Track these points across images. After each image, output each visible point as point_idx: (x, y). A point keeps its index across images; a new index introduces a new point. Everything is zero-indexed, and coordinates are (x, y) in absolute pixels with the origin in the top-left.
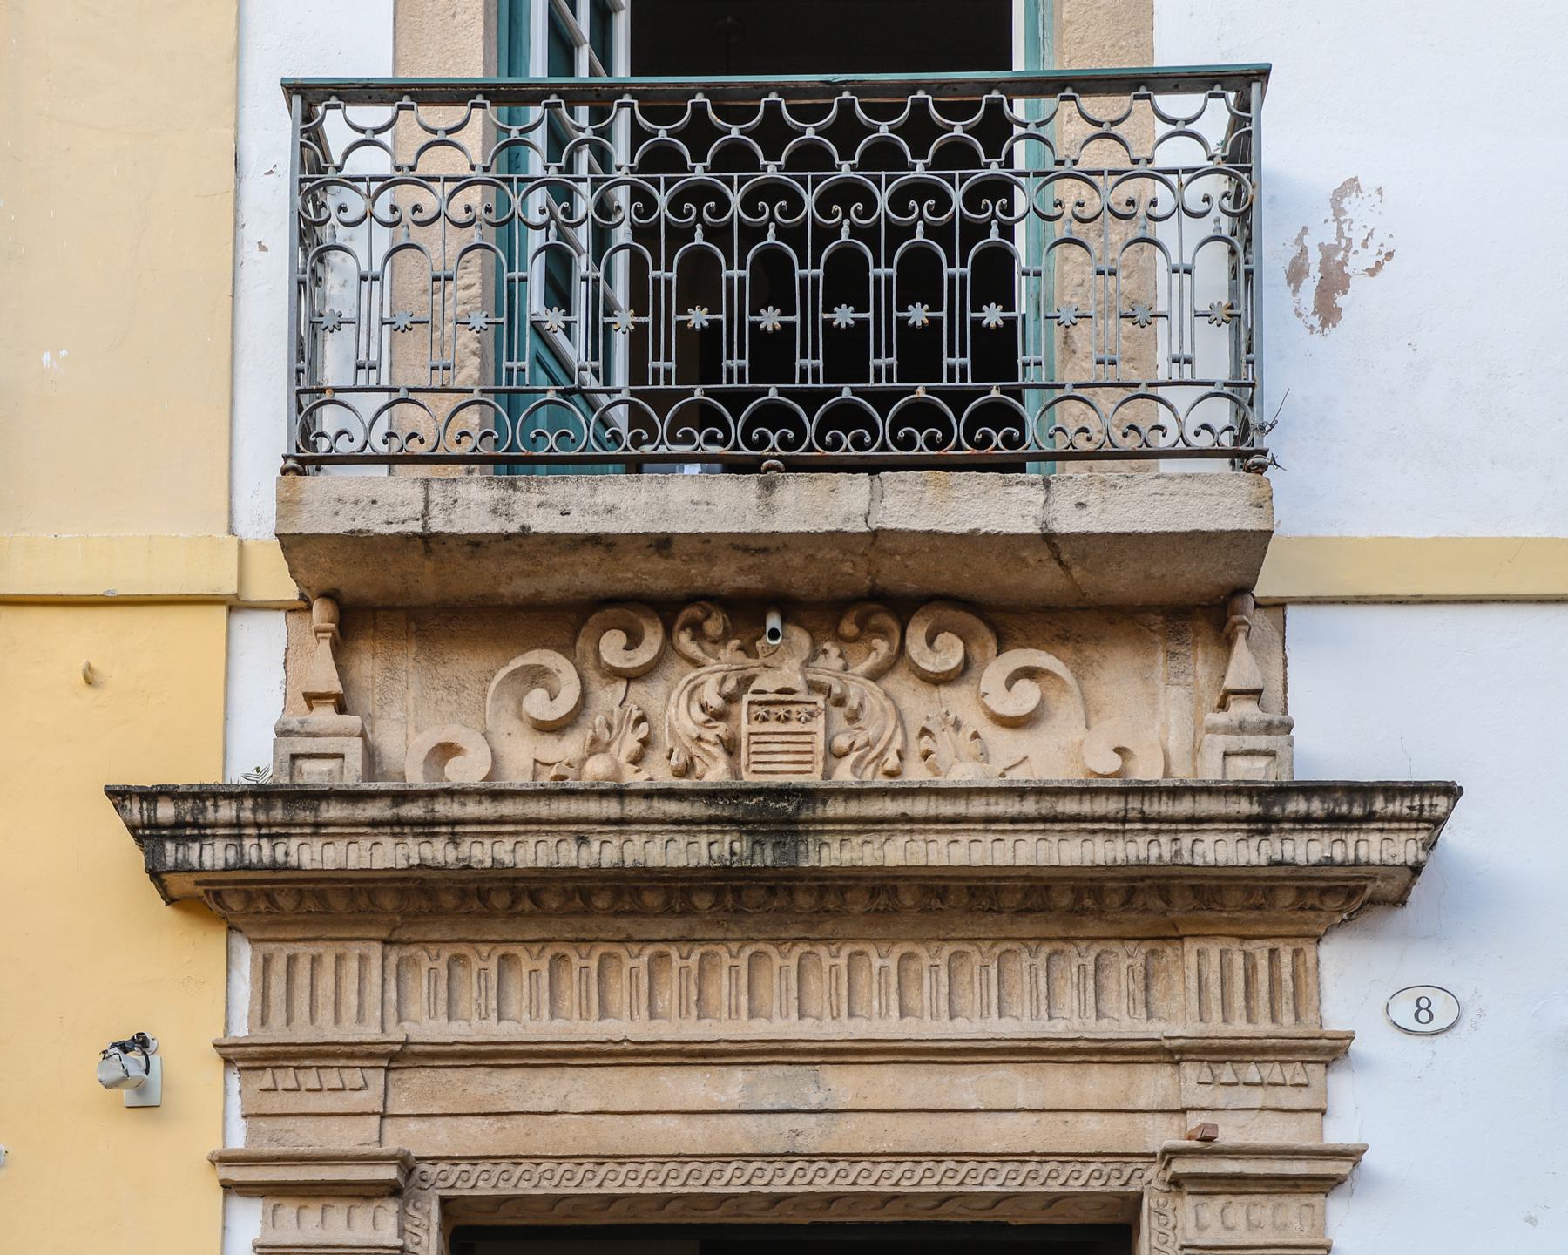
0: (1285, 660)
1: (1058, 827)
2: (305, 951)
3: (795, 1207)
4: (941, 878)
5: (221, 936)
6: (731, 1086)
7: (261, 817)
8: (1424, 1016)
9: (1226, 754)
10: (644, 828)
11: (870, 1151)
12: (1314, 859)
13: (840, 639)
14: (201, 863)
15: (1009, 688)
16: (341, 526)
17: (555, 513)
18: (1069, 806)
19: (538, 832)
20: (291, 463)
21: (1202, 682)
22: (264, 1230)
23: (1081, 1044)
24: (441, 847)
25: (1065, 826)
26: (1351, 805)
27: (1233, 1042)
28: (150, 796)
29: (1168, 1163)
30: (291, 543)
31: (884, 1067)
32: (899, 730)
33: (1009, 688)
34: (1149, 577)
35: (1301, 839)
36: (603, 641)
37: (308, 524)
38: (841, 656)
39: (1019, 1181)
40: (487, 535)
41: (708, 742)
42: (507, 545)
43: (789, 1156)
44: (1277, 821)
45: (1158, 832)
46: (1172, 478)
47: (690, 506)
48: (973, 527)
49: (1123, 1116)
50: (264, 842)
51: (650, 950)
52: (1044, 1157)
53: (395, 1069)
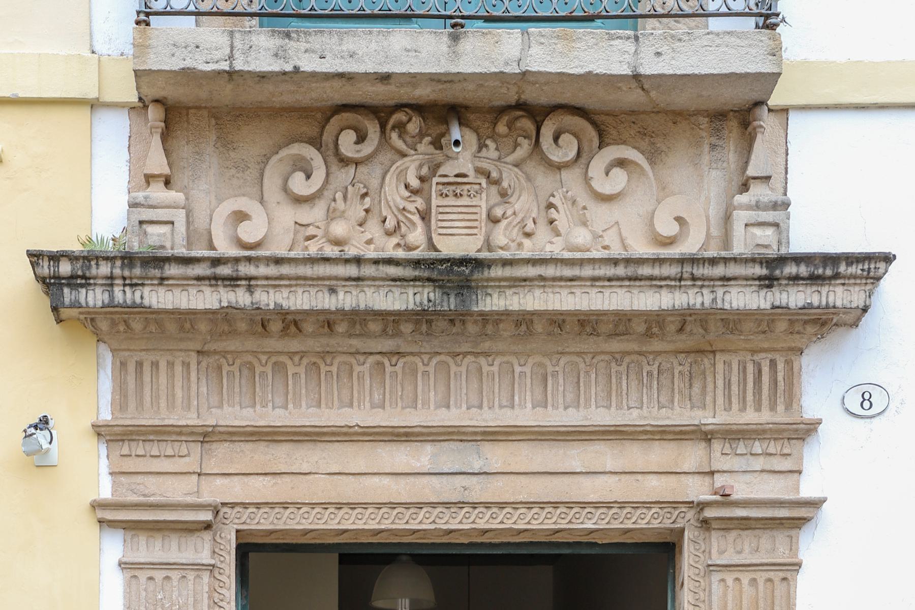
0: (787, 150)
1: (637, 283)
2: (148, 358)
3: (461, 535)
4: (562, 314)
6: (422, 457)
7: (127, 273)
8: (866, 404)
9: (746, 225)
10: (373, 283)
11: (512, 500)
12: (800, 304)
13: (494, 136)
14: (87, 303)
15: (607, 174)
16: (175, 64)
17: (315, 57)
18: (646, 271)
20: (142, 17)
21: (733, 166)
23: (648, 428)
24: (241, 294)
25: (642, 283)
26: (825, 268)
27: (745, 427)
28: (55, 258)
29: (702, 509)
31: (522, 443)
33: (607, 174)
34: (702, 96)
35: (792, 290)
37: (153, 63)
38: (497, 149)
39: (606, 520)
43: (460, 504)
44: (778, 279)
45: (702, 286)
46: (718, 34)
49: (673, 476)
50: (127, 289)
51: (371, 359)
52: (622, 505)
53: (207, 442)
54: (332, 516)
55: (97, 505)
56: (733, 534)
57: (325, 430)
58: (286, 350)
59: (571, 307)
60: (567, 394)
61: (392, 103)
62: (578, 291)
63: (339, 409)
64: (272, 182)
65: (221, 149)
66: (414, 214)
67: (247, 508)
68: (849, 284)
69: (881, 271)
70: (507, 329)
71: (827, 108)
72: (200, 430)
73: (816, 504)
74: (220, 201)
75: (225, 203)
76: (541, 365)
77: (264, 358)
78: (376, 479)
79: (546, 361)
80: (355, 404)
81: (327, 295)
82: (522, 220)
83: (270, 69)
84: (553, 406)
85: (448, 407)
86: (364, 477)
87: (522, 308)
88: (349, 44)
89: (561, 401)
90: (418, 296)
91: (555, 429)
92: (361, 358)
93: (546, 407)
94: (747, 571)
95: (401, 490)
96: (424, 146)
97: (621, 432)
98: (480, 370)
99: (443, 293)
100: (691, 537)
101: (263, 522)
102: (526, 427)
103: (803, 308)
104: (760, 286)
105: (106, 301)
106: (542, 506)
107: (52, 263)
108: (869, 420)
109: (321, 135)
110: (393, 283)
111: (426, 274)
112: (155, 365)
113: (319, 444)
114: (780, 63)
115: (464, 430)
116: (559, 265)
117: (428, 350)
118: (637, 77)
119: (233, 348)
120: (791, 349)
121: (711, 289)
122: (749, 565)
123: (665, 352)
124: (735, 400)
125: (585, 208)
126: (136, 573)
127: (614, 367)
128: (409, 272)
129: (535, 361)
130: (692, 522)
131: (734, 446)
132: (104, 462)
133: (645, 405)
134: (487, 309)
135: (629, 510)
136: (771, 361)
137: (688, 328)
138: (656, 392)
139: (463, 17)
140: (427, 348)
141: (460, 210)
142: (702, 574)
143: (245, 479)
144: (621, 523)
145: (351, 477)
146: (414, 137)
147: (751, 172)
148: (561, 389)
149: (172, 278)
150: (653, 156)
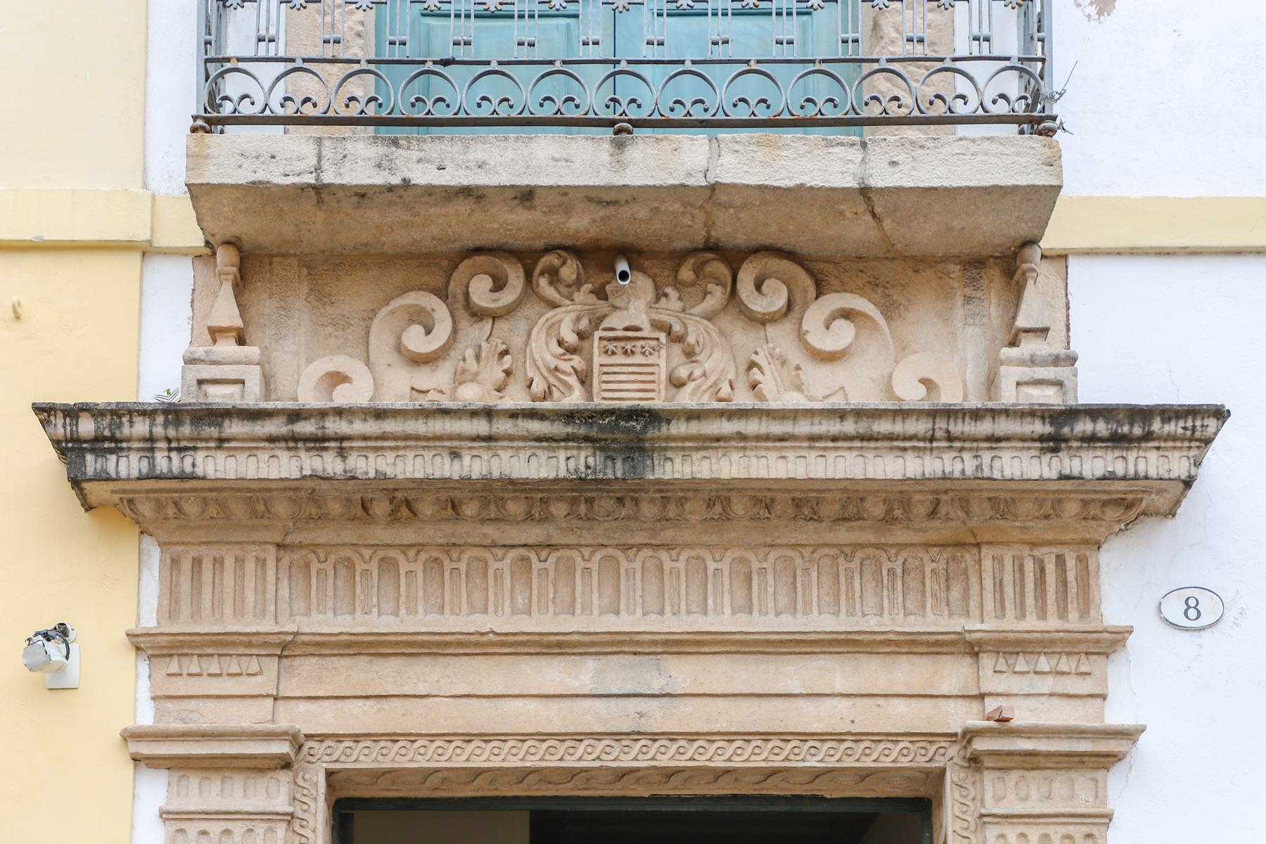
1: (873, 444)
2: (208, 554)
7: (171, 433)
8: (1192, 614)
9: (1018, 384)
10: (510, 444)
11: (706, 730)
12: (1099, 473)
13: (678, 284)
14: (117, 473)
15: (828, 328)
18: (883, 427)
20: (200, 122)
21: (996, 322)
23: (892, 637)
25: (879, 444)
26: (1132, 425)
27: (1026, 636)
28: (72, 413)
29: (969, 742)
30: (197, 192)
31: (718, 657)
33: (828, 328)
34: (951, 229)
38: (680, 299)
39: (837, 757)
43: (636, 735)
44: (1066, 440)
45: (962, 449)
50: (174, 455)
51: (513, 553)
53: (287, 657)
54: (459, 751)
55: (131, 736)
56: (1014, 776)
57: (448, 638)
58: (397, 542)
59: (782, 474)
60: (779, 597)
61: (539, 244)
62: (791, 455)
63: (468, 615)
64: (381, 340)
65: (315, 303)
66: (570, 375)
67: (341, 742)
68: (1166, 448)
69: (1211, 430)
70: (695, 512)
71: (1118, 253)
72: (275, 639)
73: (1129, 734)
74: (309, 361)
75: (316, 363)
76: (743, 561)
77: (367, 553)
78: (519, 703)
79: (750, 556)
80: (491, 609)
81: (447, 459)
82: (715, 383)
83: (370, 182)
84: (760, 611)
85: (617, 612)
86: (501, 702)
87: (714, 476)
88: (478, 152)
89: (771, 604)
91: (764, 637)
92: (500, 552)
93: (751, 613)
94: (1036, 824)
96: (583, 295)
97: (855, 642)
98: (660, 567)
99: (607, 458)
100: (956, 779)
101: (366, 759)
102: (723, 633)
103: (1104, 478)
104: (1042, 449)
105: (145, 471)
106: (747, 738)
107: (68, 420)
108: (1196, 634)
109: (448, 283)
110: (537, 444)
111: (582, 431)
112: (218, 562)
113: (441, 659)
114: (1059, 175)
115: (638, 637)
116: (764, 418)
117: (590, 541)
118: (865, 192)
119: (323, 540)
120: (1085, 542)
121: (975, 453)
122: (1039, 816)
123: (912, 545)
124: (1009, 605)
125: (798, 368)
126: (183, 825)
127: (843, 564)
128: (558, 429)
129: (735, 555)
130: (955, 760)
131: (1011, 662)
132: (144, 684)
133: (886, 612)
134: (667, 477)
135: (867, 744)
136: (1058, 556)
137: (943, 510)
138: (900, 595)
139: (629, 121)
140: (588, 538)
142: (972, 828)
143: (339, 703)
144: (857, 760)
145: (484, 700)
146: (569, 286)
147: (1021, 322)
148: (771, 590)
149: (236, 439)
150: (890, 310)
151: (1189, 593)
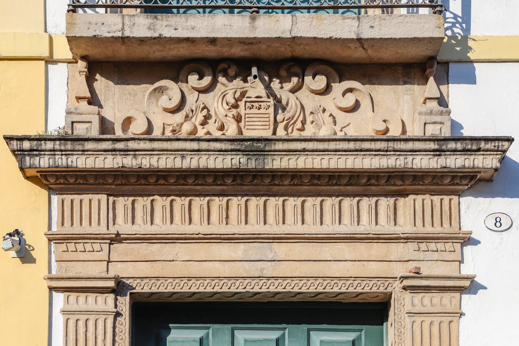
5: (45, 193)
6: (239, 250)
7: (63, 148)
8: (498, 224)
11: (290, 276)
15: (343, 97)
16: (90, 33)
19: (167, 154)
20: (71, 8)
22: (64, 305)
26: (472, 145)
29: (402, 281)
30: (71, 40)
32: (302, 113)
34: (398, 53)
35: (453, 158)
36: (189, 77)
40: (146, 37)
41: (230, 117)
42: (154, 41)
47: (223, 27)
48: (331, 35)
50: (63, 157)
90: (233, 160)
94: (429, 316)
95: (226, 270)
135: (359, 282)
141: (260, 116)
151: (497, 215)
